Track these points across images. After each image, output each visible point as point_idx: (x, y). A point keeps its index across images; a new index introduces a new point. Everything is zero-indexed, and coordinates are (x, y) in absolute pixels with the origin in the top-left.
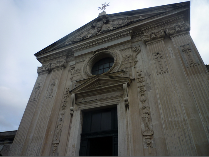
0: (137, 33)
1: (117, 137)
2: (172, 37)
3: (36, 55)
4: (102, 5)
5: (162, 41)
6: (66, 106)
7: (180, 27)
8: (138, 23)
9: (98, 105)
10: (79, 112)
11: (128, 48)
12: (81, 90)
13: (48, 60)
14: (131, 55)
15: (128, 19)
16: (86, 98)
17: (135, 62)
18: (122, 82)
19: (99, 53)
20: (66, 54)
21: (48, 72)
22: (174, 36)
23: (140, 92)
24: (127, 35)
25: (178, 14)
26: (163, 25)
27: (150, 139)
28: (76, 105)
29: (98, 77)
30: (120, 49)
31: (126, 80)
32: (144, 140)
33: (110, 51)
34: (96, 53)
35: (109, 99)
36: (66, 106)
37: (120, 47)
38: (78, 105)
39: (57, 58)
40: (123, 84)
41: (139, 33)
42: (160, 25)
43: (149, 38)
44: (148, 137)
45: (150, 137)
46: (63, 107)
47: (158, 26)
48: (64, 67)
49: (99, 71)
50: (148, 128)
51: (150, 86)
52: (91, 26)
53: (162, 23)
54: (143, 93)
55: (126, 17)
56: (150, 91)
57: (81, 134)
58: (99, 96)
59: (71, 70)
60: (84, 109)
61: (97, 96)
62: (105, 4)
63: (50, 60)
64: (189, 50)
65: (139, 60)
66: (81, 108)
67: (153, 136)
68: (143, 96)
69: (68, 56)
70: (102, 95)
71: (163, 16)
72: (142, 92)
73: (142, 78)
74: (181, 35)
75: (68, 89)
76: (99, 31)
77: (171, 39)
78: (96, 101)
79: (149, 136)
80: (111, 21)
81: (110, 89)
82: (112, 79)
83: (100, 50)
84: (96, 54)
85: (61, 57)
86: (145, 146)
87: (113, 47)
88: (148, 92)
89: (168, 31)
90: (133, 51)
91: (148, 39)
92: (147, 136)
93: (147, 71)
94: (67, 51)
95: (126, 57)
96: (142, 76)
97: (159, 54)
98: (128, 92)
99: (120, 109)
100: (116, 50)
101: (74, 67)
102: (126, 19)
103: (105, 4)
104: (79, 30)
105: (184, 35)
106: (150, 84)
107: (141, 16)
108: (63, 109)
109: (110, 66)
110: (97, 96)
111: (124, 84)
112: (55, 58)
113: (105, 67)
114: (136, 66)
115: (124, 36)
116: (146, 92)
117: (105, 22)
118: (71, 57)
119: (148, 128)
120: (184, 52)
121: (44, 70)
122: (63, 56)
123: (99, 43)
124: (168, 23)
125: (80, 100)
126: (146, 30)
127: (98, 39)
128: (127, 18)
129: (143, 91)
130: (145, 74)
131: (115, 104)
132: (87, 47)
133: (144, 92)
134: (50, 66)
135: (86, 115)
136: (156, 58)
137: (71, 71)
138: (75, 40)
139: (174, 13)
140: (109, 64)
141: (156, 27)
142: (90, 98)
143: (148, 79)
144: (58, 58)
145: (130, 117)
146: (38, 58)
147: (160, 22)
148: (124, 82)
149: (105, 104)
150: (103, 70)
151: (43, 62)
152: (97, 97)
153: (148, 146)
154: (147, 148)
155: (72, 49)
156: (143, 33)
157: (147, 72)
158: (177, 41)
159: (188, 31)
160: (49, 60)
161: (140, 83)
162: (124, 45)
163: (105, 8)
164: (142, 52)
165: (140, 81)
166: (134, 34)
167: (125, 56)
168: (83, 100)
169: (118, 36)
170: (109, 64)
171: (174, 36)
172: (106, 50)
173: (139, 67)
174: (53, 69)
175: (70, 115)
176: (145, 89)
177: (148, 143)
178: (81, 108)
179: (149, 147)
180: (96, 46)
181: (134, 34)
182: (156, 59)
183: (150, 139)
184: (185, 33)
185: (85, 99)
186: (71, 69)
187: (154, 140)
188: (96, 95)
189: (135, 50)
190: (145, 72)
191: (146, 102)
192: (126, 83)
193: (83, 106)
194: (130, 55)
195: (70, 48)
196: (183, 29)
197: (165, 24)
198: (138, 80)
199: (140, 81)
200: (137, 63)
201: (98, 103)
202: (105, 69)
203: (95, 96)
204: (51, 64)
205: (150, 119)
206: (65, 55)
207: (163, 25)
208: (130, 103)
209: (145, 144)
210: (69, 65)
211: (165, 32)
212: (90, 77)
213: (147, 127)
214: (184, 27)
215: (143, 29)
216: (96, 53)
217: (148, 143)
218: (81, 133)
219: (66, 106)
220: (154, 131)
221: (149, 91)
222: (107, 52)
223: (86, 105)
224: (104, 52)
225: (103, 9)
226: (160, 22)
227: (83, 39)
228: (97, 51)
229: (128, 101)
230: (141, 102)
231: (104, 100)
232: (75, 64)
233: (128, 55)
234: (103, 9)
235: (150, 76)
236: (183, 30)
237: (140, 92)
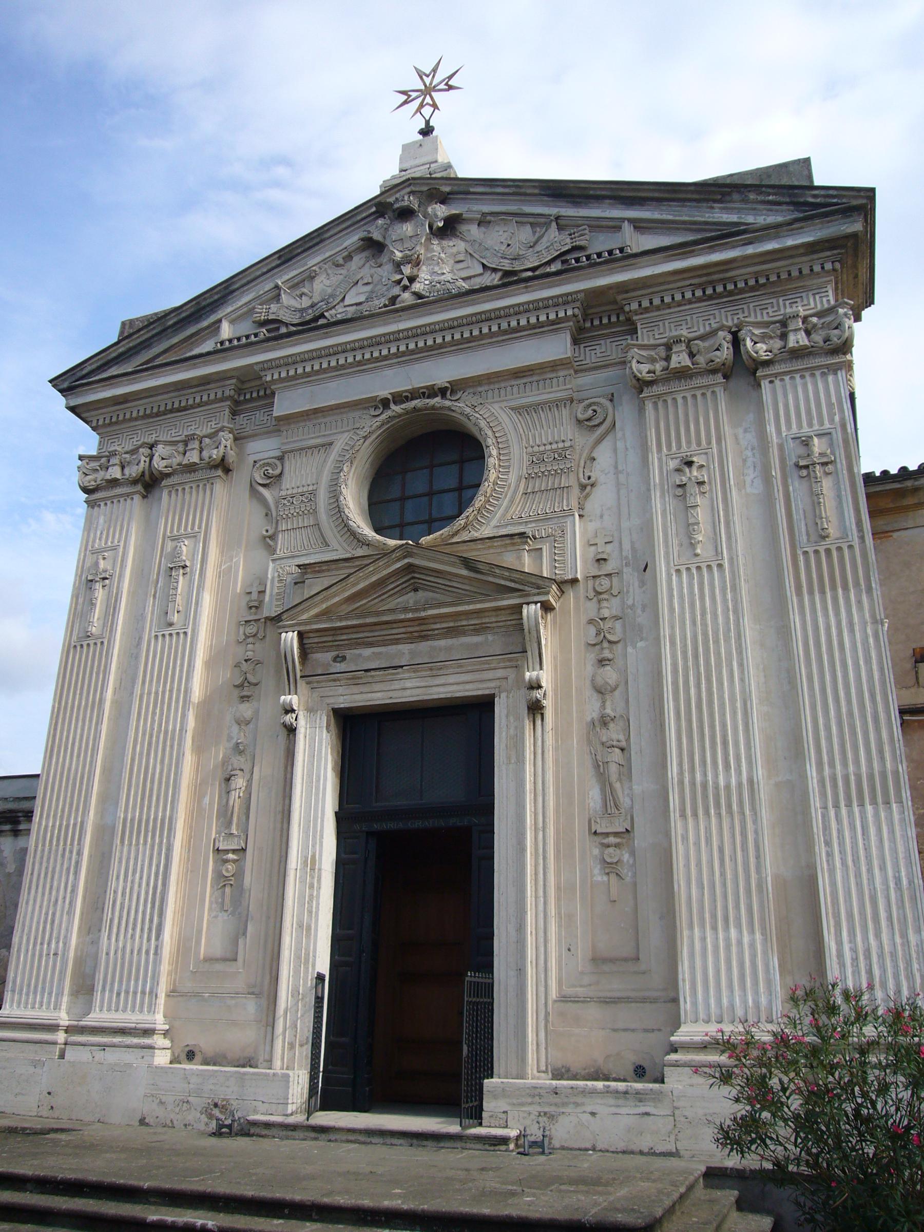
0: (605, 321)
1: (492, 832)
2: (765, 377)
3: (50, 381)
4: (421, 75)
5: (717, 389)
6: (256, 684)
7: (809, 327)
8: (611, 272)
9: (408, 692)
10: (325, 719)
11: (557, 404)
12: (325, 614)
13: (132, 419)
14: (567, 444)
15: (560, 228)
16: (349, 653)
17: (583, 487)
18: (520, 597)
19: (407, 412)
20: (227, 393)
21: (140, 493)
22: (776, 375)
23: (594, 645)
24: (554, 325)
25: (812, 248)
26: (731, 293)
27: (617, 846)
28: (308, 683)
29: (405, 557)
30: (513, 404)
31: (538, 588)
32: (596, 851)
33: (462, 407)
34: (393, 406)
35: (459, 670)
36: (254, 681)
37: (515, 389)
38: (315, 685)
39: (179, 410)
40: (520, 606)
41: (614, 319)
42: (720, 296)
43: (658, 367)
44: (612, 840)
45: (618, 840)
46: (240, 686)
47: (710, 298)
48: (223, 466)
49: (409, 505)
50: (616, 806)
51: (639, 620)
52: (362, 239)
53: (730, 287)
54: (607, 654)
55: (554, 211)
56: (640, 644)
57: (336, 813)
58: (413, 646)
59: (261, 489)
60: (347, 705)
61: (400, 647)
62: (435, 70)
63: (145, 416)
64: (826, 464)
65: (602, 479)
66: (331, 700)
67: (632, 834)
68: (608, 668)
69: (237, 403)
70: (424, 646)
71: (734, 247)
72: (605, 644)
73: (609, 575)
74: (807, 374)
75: (255, 596)
76: (406, 282)
77: (759, 385)
78: (398, 674)
79: (616, 834)
80: (470, 221)
81: (464, 623)
82: (472, 575)
83: (414, 394)
84: (389, 413)
85: (199, 405)
86: (596, 871)
87: (480, 385)
88: (630, 650)
89: (749, 344)
90: (579, 422)
91: (652, 368)
92: (607, 835)
93: (632, 543)
94: (231, 378)
95: (543, 453)
96: (609, 568)
97: (694, 468)
98: (543, 642)
99: (507, 716)
100: (496, 406)
101: (278, 472)
102: (554, 224)
103: (435, 70)
104: (287, 255)
105: (818, 373)
106: (639, 611)
107: (630, 220)
108: (244, 698)
109: (465, 484)
110: (405, 648)
111: (528, 604)
112: (172, 411)
113: (436, 488)
114: (589, 506)
115: (536, 329)
116: (620, 646)
117: (439, 229)
118: (258, 408)
119: (616, 806)
120: (804, 472)
121: (119, 476)
122: (217, 401)
123: (404, 354)
124: (758, 286)
125: (323, 658)
126: (646, 310)
127: (399, 332)
128: (557, 218)
129: (610, 642)
130: (626, 557)
131: (487, 692)
132: (343, 367)
133: (614, 647)
134: (151, 457)
135: (357, 731)
136: (679, 486)
137: (258, 492)
138: (271, 317)
139: (790, 242)
140: (455, 468)
141: (700, 300)
142: (367, 656)
143: (636, 584)
144: (185, 409)
145: (550, 755)
146: (72, 404)
147: (721, 276)
148: (528, 595)
149: (441, 689)
150: (426, 499)
151: (104, 425)
152: (404, 652)
153: (608, 874)
154: (605, 878)
155: (264, 370)
156: (634, 331)
157: (634, 549)
158: (790, 402)
159: (848, 357)
160: (136, 419)
161: (599, 601)
162: (535, 378)
163: (435, 106)
164: (619, 434)
165: (601, 593)
166: (588, 325)
167: (536, 449)
168: (335, 659)
169: (504, 326)
170: (455, 468)
171: (776, 375)
172: (444, 396)
173: (601, 517)
174: (168, 475)
175: (283, 733)
176: (617, 631)
177: (608, 863)
178: (331, 700)
179: (613, 877)
180: (391, 366)
181: (588, 325)
182: (679, 491)
183: (617, 846)
184: (827, 366)
185: (344, 658)
186: (264, 485)
187: (633, 853)
188: (396, 642)
189: (589, 420)
190: (627, 546)
191: (617, 693)
192: (536, 603)
193: (341, 690)
194: (561, 445)
195: (251, 366)
196: (822, 343)
197: (742, 291)
198: (590, 583)
199: (601, 593)
200: (594, 489)
201: (408, 684)
202: (435, 499)
203: (392, 649)
204: (151, 447)
205: (626, 770)
206: (222, 400)
207: (731, 293)
208: (550, 694)
209: (599, 867)
210: (251, 459)
211: (736, 342)
212: (360, 552)
213: (610, 802)
214: (823, 333)
215: (634, 306)
216: (393, 406)
217: (609, 860)
218: (337, 809)
219: (256, 684)
220: (636, 819)
221: (635, 647)
222: (449, 409)
223: (355, 689)
224: (433, 408)
225: (427, 111)
226: (721, 276)
227: (313, 324)
228: (399, 398)
229: (540, 687)
230: (595, 694)
231: (434, 672)
232: (277, 453)
233: (554, 446)
234: (422, 106)
235: (645, 570)
236: (822, 348)
237: (598, 647)
